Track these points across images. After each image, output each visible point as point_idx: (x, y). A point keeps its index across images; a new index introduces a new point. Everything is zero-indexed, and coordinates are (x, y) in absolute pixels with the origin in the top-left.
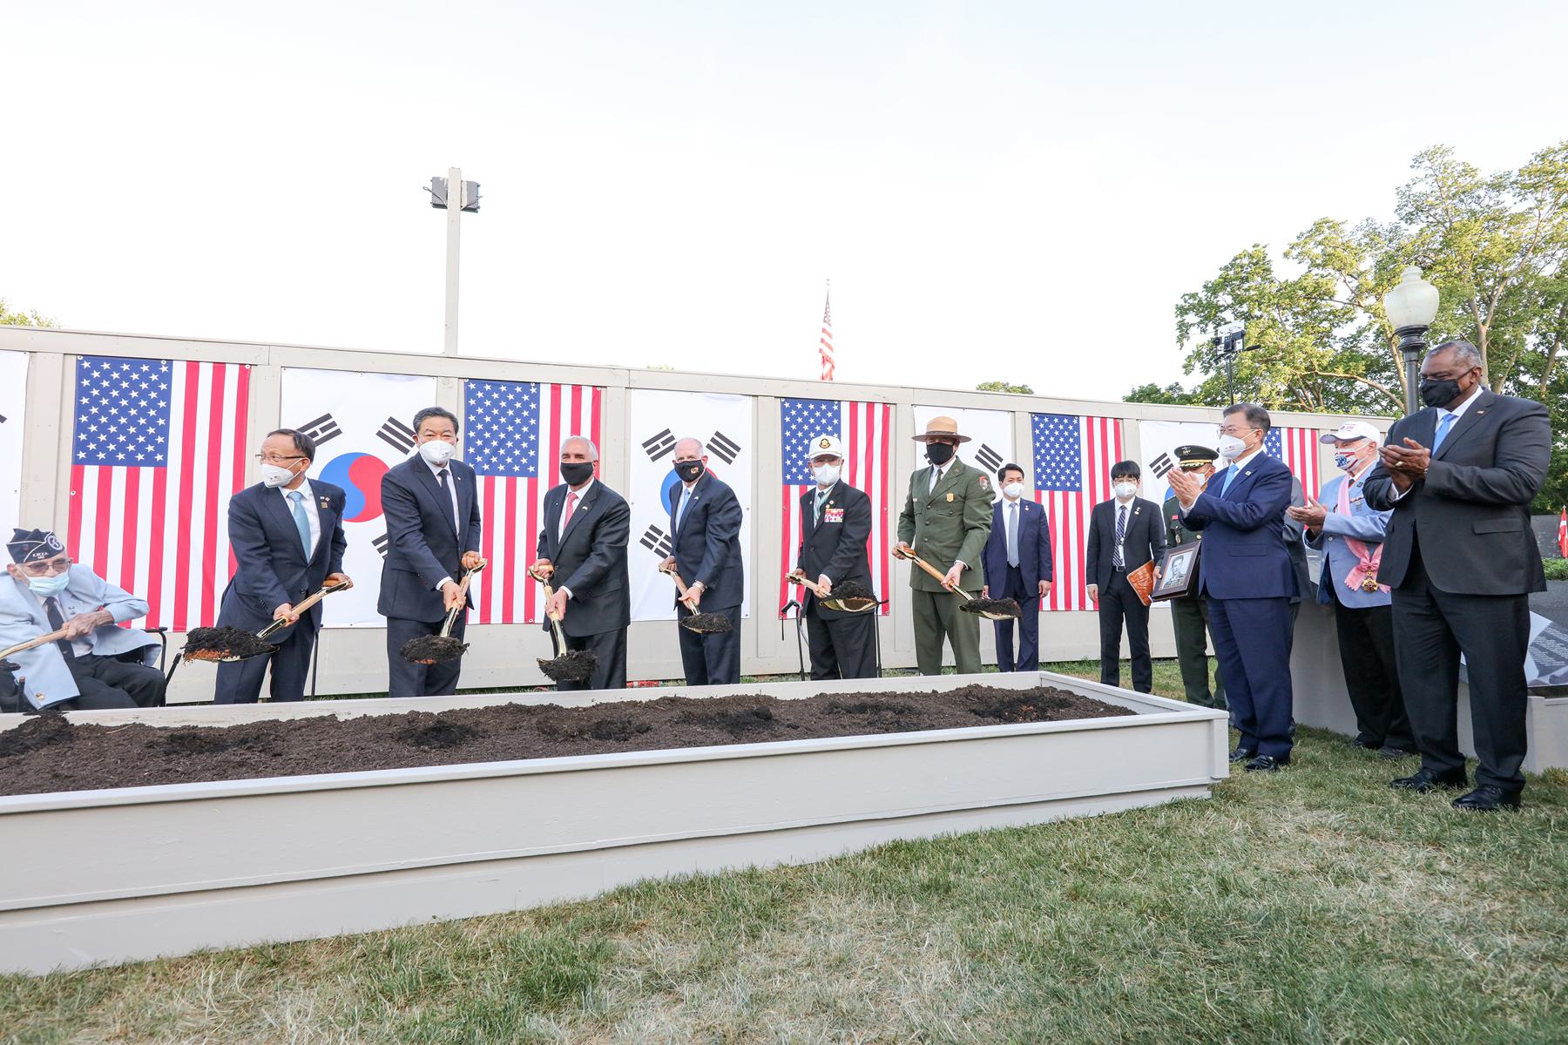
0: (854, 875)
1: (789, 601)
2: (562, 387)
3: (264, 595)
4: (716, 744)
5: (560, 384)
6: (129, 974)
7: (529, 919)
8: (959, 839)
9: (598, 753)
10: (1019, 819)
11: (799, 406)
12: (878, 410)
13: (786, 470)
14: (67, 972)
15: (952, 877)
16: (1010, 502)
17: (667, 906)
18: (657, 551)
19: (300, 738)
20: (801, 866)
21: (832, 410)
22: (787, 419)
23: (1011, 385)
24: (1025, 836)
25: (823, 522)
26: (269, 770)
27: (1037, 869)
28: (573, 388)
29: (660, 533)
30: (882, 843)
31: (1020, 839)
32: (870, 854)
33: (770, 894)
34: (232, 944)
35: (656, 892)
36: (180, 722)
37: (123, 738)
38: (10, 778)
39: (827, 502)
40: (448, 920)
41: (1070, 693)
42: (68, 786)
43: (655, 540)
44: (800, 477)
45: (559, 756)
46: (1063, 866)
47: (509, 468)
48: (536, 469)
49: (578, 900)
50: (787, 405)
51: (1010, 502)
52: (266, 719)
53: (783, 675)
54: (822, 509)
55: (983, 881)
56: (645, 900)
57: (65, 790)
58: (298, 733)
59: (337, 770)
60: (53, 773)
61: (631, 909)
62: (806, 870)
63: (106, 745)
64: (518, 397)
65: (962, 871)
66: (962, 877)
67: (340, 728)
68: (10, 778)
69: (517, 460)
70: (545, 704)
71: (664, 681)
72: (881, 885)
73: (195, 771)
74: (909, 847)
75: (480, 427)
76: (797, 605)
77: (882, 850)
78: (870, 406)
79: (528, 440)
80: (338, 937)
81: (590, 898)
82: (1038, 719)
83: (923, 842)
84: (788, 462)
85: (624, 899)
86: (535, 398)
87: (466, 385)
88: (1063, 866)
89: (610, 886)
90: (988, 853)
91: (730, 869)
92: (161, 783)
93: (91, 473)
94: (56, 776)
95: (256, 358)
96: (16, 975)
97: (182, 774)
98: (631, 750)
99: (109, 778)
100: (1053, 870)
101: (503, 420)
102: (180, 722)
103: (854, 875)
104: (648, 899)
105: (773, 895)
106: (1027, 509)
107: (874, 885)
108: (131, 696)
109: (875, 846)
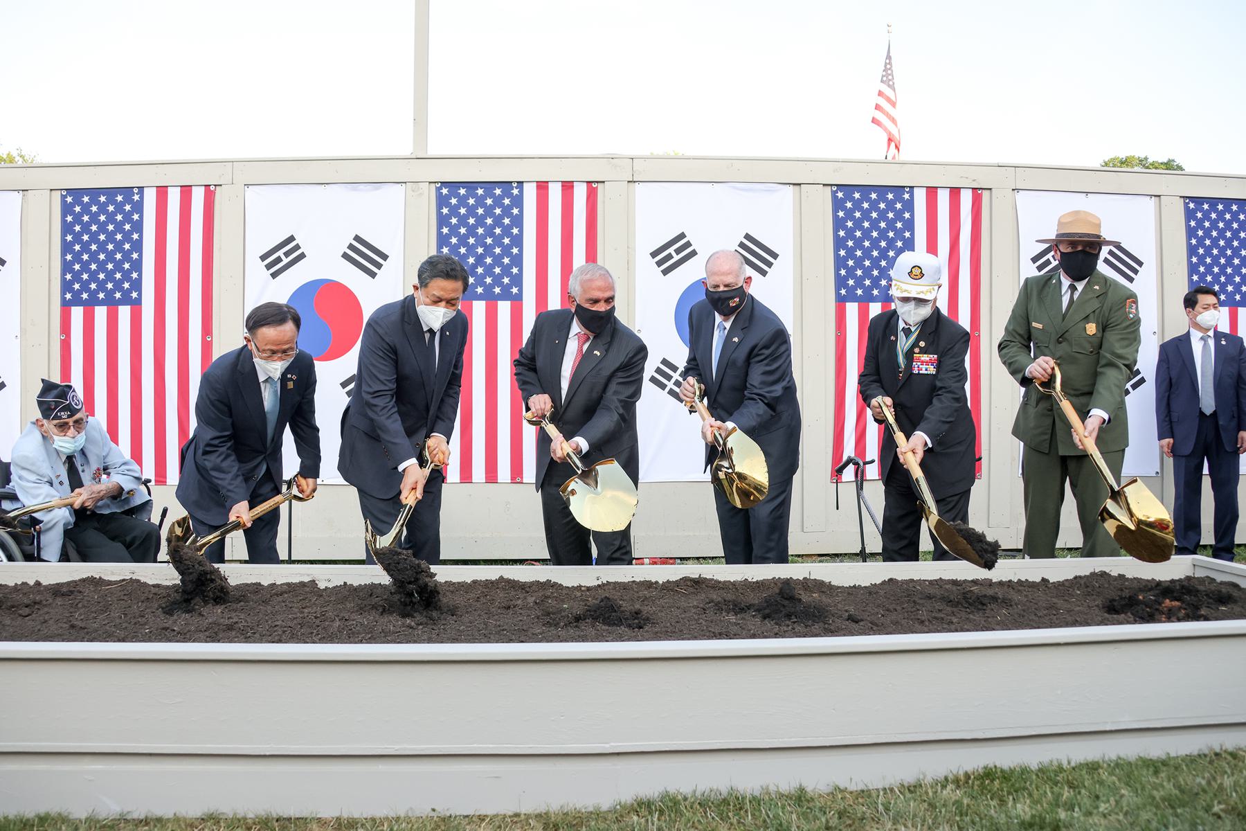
0: (932, 806)
1: (845, 458)
2: (550, 184)
3: (223, 487)
4: (753, 636)
5: (547, 182)
6: (152, 827)
7: (536, 824)
8: (1074, 769)
9: (607, 641)
10: (1155, 747)
11: (874, 196)
12: (966, 199)
13: (66, 286)
14: (101, 818)
15: (1062, 815)
16: (1201, 335)
17: (696, 824)
18: (672, 392)
19: (283, 604)
20: (863, 791)
21: (902, 200)
22: (842, 253)
23: (1150, 160)
24: (1165, 769)
25: (912, 374)
26: (257, 635)
27: (1179, 811)
28: (562, 186)
29: (674, 369)
30: (969, 768)
31: (1156, 772)
32: (953, 782)
33: (823, 820)
34: (238, 811)
35: (683, 808)
36: (170, 580)
37: (123, 593)
38: (36, 626)
39: (915, 344)
40: (449, 815)
41: (1236, 586)
42: (83, 638)
43: (669, 378)
44: (859, 292)
45: (561, 641)
46: (1216, 809)
47: (488, 289)
48: (521, 290)
49: (591, 809)
50: (840, 195)
51: (1201, 335)
52: (249, 582)
53: (837, 555)
54: (909, 355)
55: (1103, 821)
56: (669, 816)
57: (82, 641)
58: (280, 598)
59: (323, 640)
60: (70, 624)
61: (653, 824)
62: (870, 796)
63: (110, 599)
64: (498, 201)
65: (1077, 809)
66: (1075, 815)
67: (321, 596)
68: (36, 626)
69: (118, 286)
70: (542, 581)
71: (681, 559)
72: (968, 819)
73: (189, 631)
74: (1006, 776)
75: (454, 240)
76: (856, 464)
77: (969, 778)
78: (955, 192)
79: (510, 255)
80: (338, 819)
81: (605, 807)
82: (1188, 618)
83: (1025, 771)
84: (843, 272)
85: (644, 812)
86: (518, 201)
87: (438, 189)
88: (1216, 809)
89: (627, 795)
90: (1114, 790)
91: (772, 788)
92: (160, 641)
93: (77, 313)
94: (73, 626)
95: (220, 177)
96: (60, 814)
97: (178, 633)
98: (647, 640)
99: (116, 632)
100: (1201, 813)
101: (480, 231)
102: (170, 580)
103: (932, 806)
104: (673, 815)
105: (827, 821)
106: (1223, 343)
107: (958, 818)
108: (129, 552)
109: (961, 773)
